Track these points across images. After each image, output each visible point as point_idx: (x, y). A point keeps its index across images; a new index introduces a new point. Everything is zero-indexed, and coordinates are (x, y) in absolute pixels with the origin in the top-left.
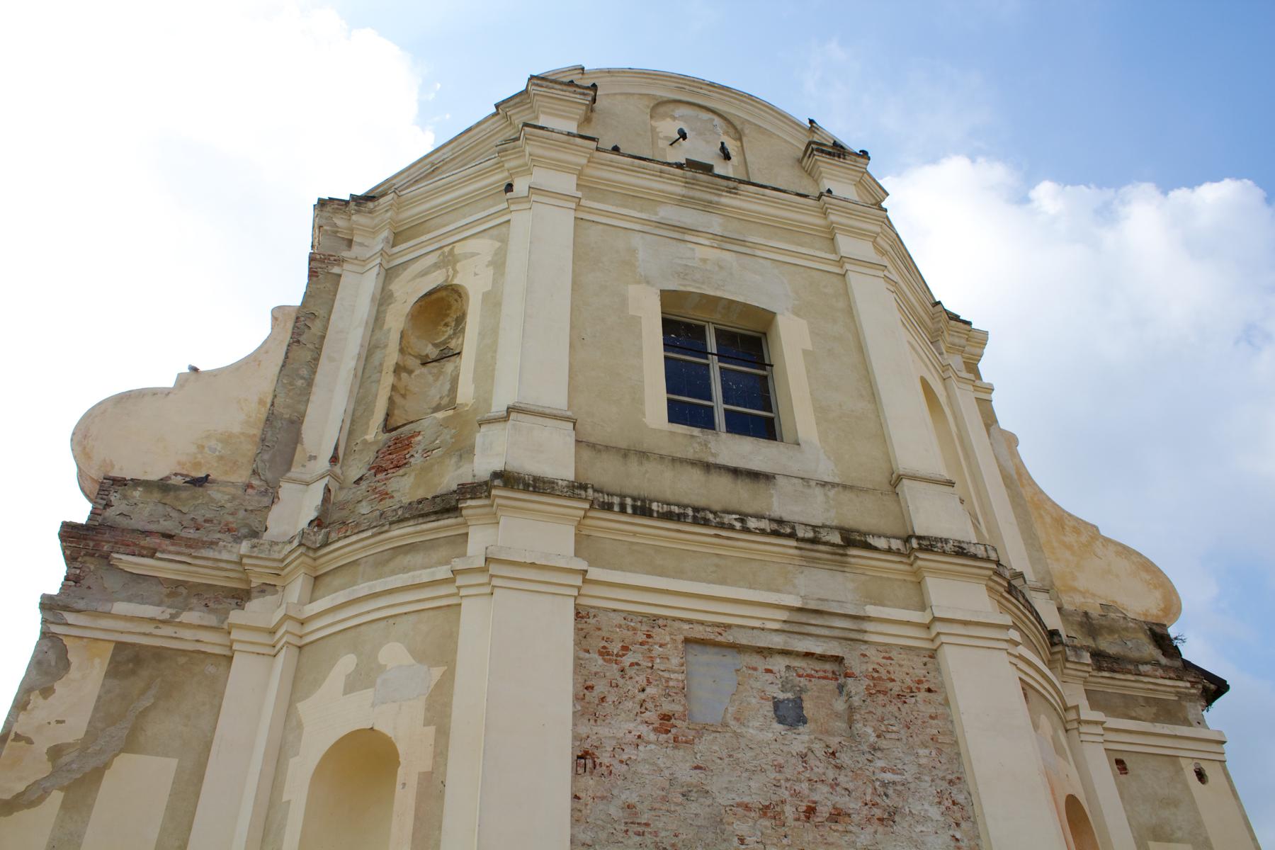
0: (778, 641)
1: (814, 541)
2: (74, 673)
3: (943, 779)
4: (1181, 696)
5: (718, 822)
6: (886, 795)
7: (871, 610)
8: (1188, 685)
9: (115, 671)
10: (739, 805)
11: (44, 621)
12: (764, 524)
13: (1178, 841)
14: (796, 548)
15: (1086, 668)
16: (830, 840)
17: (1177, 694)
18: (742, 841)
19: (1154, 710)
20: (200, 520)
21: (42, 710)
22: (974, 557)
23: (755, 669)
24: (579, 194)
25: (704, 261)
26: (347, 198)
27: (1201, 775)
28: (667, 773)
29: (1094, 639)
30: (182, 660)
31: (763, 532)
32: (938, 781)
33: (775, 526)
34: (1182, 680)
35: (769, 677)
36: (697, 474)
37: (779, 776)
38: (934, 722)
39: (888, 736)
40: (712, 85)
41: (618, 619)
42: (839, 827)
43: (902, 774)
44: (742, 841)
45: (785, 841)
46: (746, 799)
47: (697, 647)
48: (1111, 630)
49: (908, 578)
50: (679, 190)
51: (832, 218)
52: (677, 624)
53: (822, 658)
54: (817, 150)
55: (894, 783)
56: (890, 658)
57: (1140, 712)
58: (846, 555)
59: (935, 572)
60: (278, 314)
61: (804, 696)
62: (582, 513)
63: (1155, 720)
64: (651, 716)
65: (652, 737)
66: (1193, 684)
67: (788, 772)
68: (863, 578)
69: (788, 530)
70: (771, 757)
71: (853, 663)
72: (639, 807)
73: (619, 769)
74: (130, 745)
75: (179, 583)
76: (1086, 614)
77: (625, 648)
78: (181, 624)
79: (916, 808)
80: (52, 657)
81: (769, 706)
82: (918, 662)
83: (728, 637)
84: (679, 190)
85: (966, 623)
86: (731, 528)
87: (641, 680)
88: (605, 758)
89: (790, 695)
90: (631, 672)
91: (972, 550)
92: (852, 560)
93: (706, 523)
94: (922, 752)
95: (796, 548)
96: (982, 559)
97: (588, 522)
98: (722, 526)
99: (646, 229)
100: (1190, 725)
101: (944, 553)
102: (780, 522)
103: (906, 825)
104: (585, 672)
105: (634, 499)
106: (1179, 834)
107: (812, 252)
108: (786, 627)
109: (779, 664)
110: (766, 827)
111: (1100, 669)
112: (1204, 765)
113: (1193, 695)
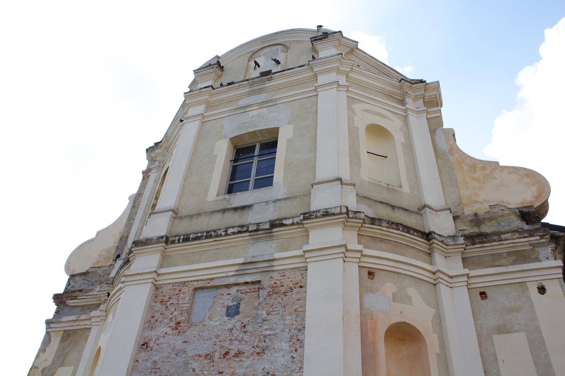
0: (232, 280)
1: (257, 230)
2: (52, 343)
3: (295, 329)
4: (534, 245)
5: (186, 364)
6: (265, 341)
7: (277, 256)
8: (538, 238)
9: (63, 340)
10: (196, 355)
11: (47, 328)
12: (235, 230)
13: (516, 331)
14: (249, 236)
15: (461, 246)
16: (232, 365)
17: (531, 245)
18: (194, 370)
19: (514, 258)
20: (94, 282)
21: (43, 356)
22: (334, 214)
23: (223, 295)
24: (348, 84)
25: (252, 117)
26: (153, 145)
27: (542, 290)
28: (172, 346)
29: (479, 227)
30: (81, 332)
31: (234, 233)
32: (293, 331)
33: (240, 229)
34: (533, 236)
35: (228, 297)
36: (219, 215)
37: (216, 340)
38: (298, 302)
39: (272, 313)
40: (276, 33)
41: (170, 287)
42: (238, 359)
43: (275, 330)
44: (194, 370)
45: (212, 368)
46: (200, 353)
47: (200, 291)
48: (491, 219)
49: (305, 234)
50: (247, 90)
51: (315, 70)
52: (192, 283)
53: (253, 283)
54: (314, 41)
55: (270, 335)
56: (285, 276)
57: (503, 261)
58: (272, 232)
59: (314, 228)
60: (130, 198)
61: (241, 302)
62: (360, 225)
63: (514, 263)
64: (173, 324)
65: (171, 332)
66: (542, 237)
67: (221, 338)
68: (281, 240)
69: (245, 229)
70: (216, 332)
71: (266, 282)
72: (158, 361)
73: (156, 347)
74: (62, 364)
75: (84, 306)
76: (476, 214)
77: (170, 298)
78: (81, 320)
79: (277, 345)
80: (47, 339)
81: (225, 310)
82: (299, 274)
83: (212, 284)
84: (247, 90)
85: (321, 249)
86: (221, 235)
87: (173, 310)
88: (151, 344)
89: (235, 303)
90: (170, 307)
91: (333, 211)
92: (275, 234)
93: (210, 237)
94: (287, 318)
95: (249, 236)
96: (337, 214)
97: (167, 250)
98: (217, 236)
99: (230, 114)
100: (540, 261)
101: (316, 217)
102: (242, 226)
103: (269, 354)
104: (153, 311)
105: (184, 236)
106: (517, 328)
107: (303, 91)
108: (237, 273)
109: (235, 289)
110: (205, 364)
111: (474, 244)
112: (545, 283)
113: (543, 242)
